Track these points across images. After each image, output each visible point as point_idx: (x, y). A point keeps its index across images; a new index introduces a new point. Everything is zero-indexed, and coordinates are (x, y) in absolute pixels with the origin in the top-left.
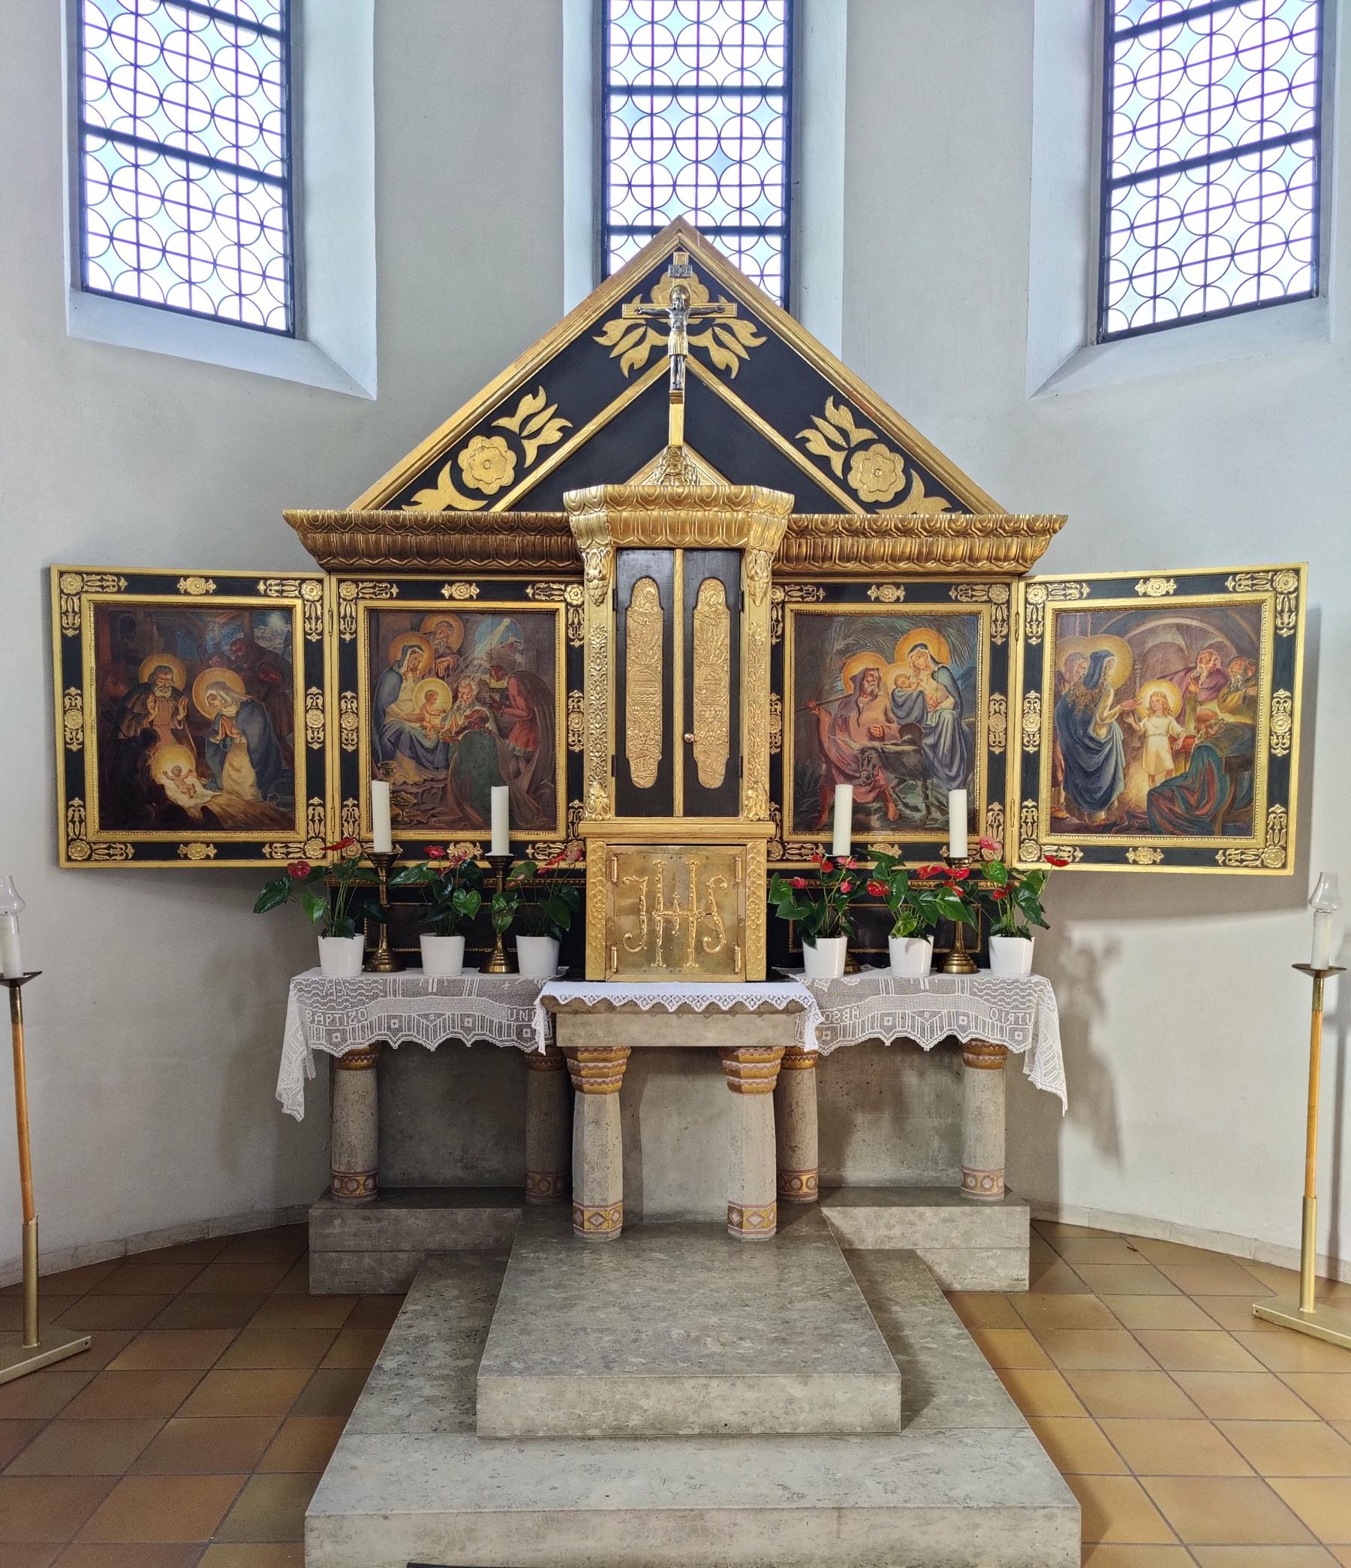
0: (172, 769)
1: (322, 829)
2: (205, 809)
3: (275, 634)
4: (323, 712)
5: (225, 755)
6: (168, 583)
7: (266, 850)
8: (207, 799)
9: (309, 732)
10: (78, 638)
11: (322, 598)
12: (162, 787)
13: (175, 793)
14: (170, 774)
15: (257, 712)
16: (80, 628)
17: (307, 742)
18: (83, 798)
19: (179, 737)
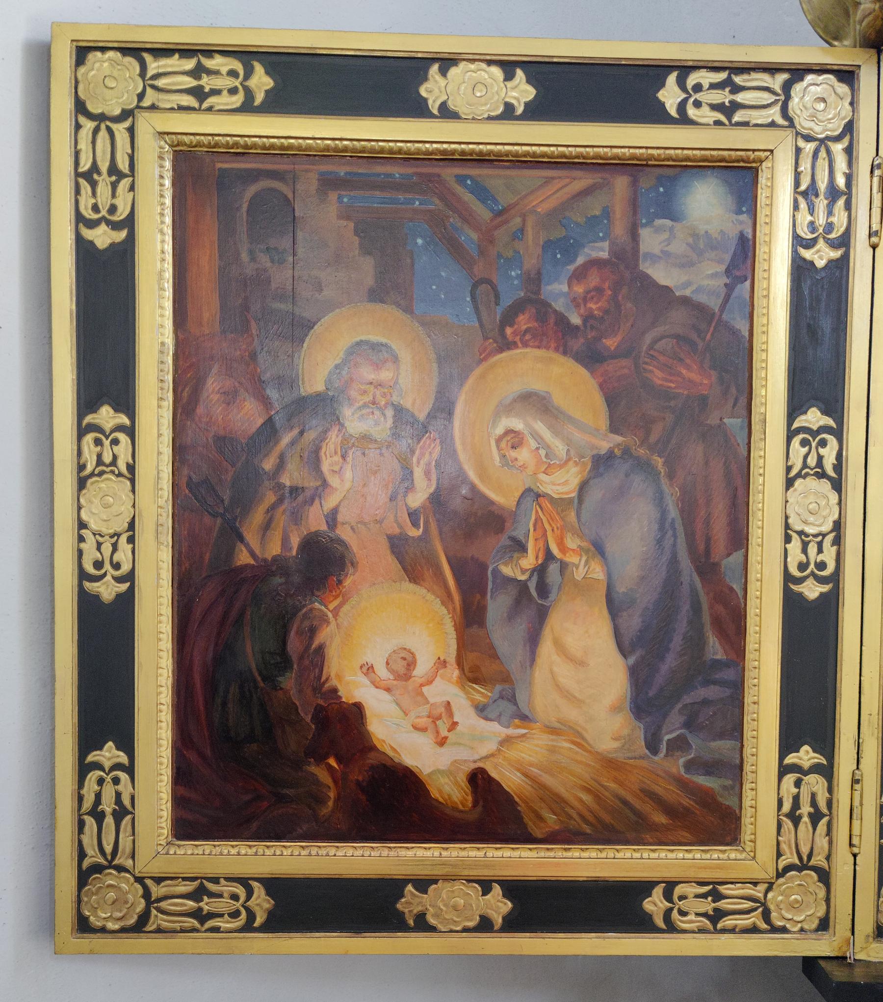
0: (387, 661)
1: (822, 842)
2: (480, 780)
3: (701, 244)
4: (838, 485)
5: (542, 615)
6: (391, 82)
7: (655, 904)
8: (484, 751)
9: (795, 546)
10: (124, 254)
11: (849, 128)
12: (358, 709)
13: (395, 731)
14: (382, 672)
15: (638, 482)
16: (129, 222)
17: (788, 578)
18: (127, 744)
19: (411, 563)
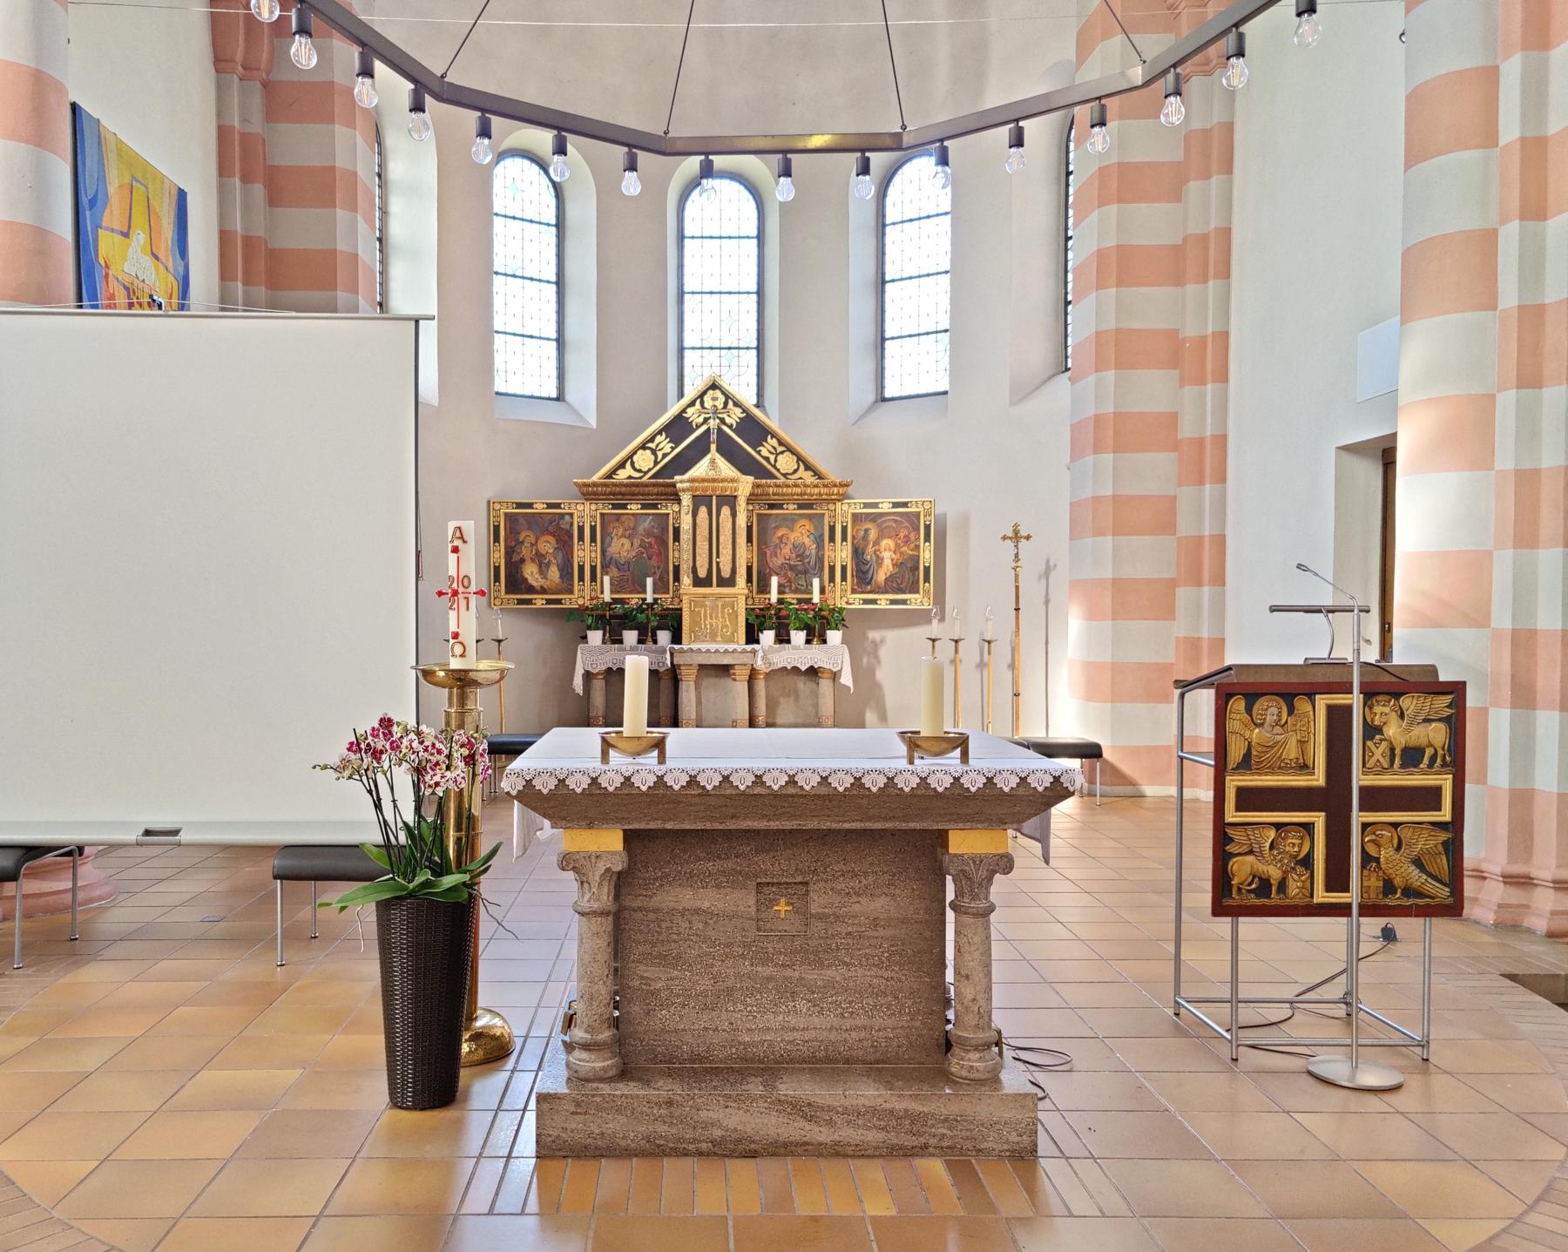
0: (530, 572)
13: (531, 581)
19: (533, 560)
